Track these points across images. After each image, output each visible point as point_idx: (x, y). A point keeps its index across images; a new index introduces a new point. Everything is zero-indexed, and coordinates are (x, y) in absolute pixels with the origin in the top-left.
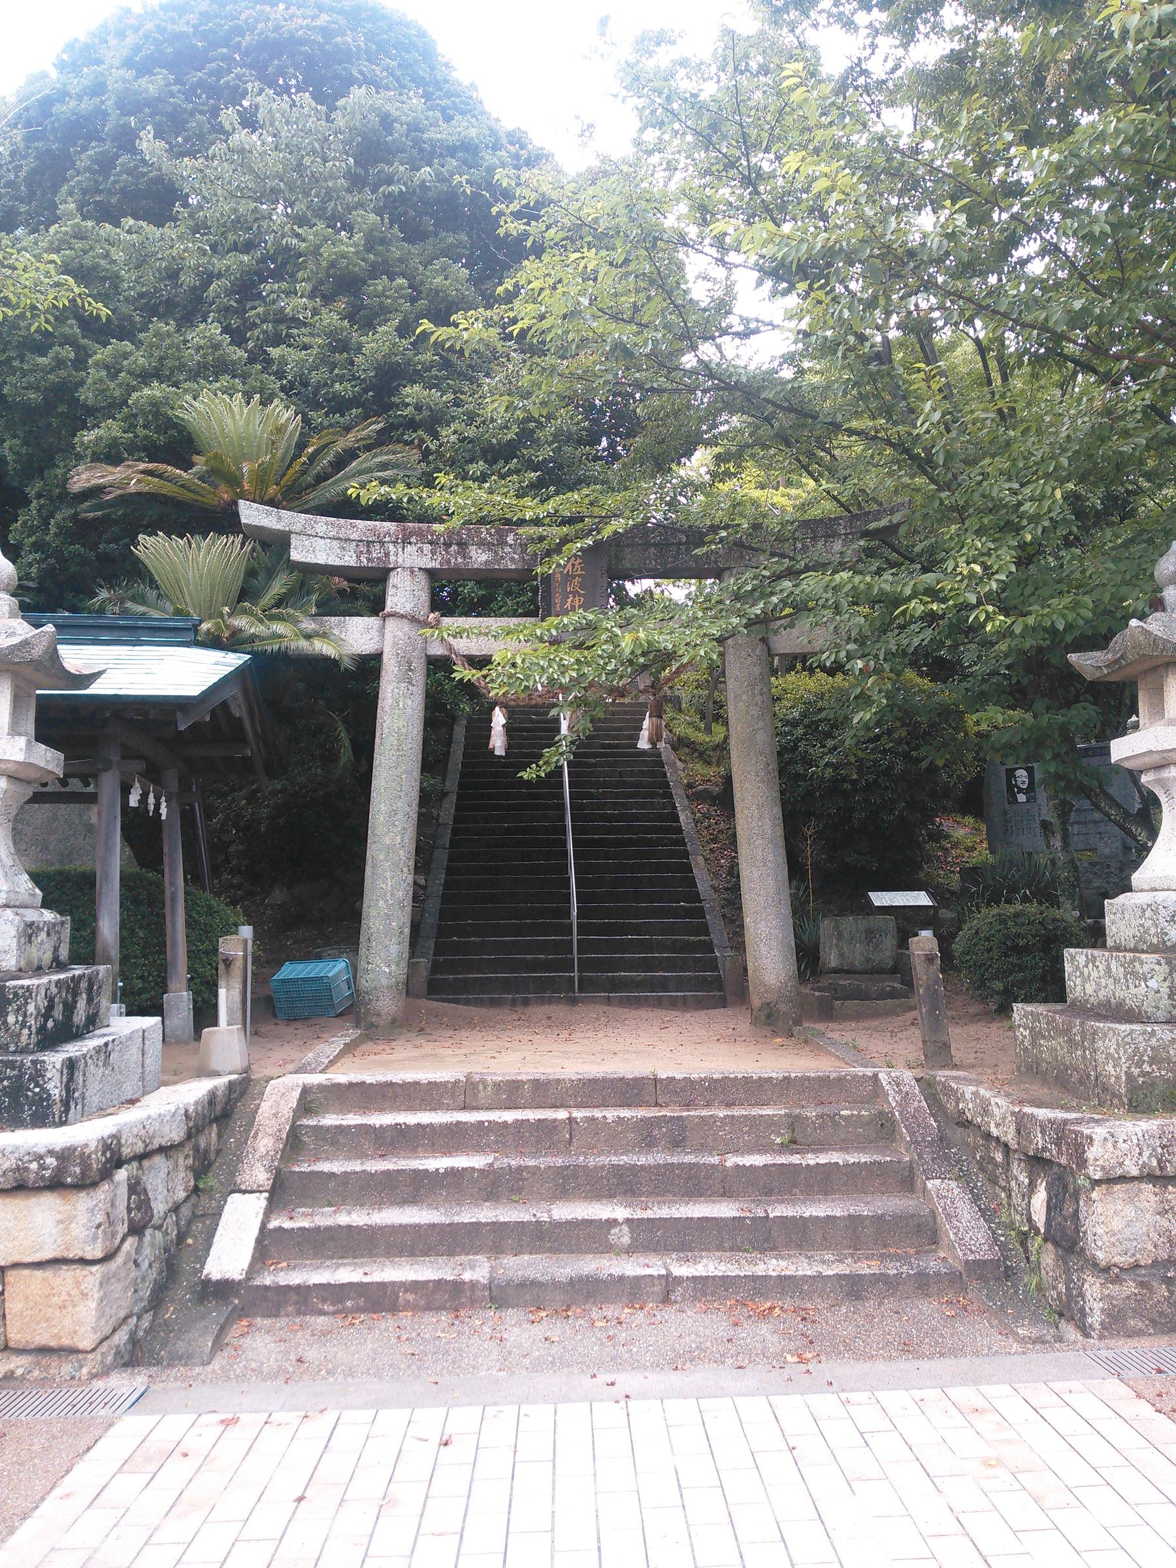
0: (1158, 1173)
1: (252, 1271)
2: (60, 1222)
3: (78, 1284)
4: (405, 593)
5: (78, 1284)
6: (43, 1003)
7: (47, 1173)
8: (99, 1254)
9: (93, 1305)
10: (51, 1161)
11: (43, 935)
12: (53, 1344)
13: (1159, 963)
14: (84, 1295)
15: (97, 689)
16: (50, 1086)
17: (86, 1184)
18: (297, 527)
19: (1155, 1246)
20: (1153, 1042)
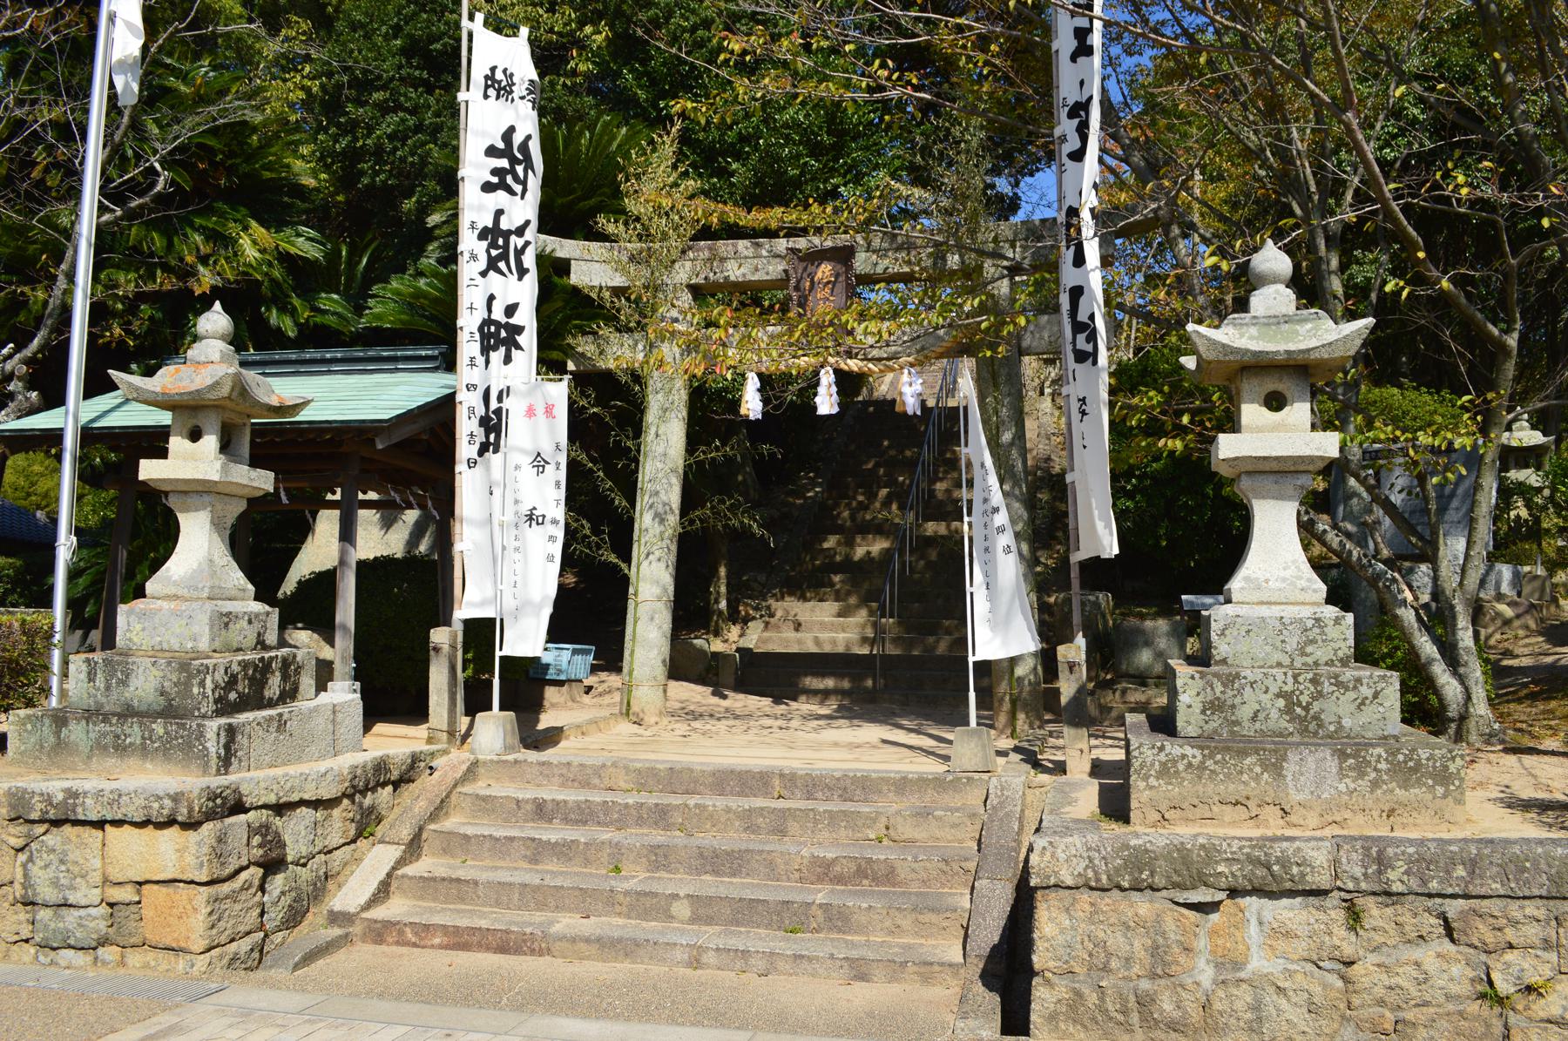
0: (1093, 884)
1: (368, 906)
2: (178, 851)
3: (190, 900)
4: (678, 311)
5: (190, 900)
6: (220, 677)
7: (165, 812)
8: (204, 879)
9: (201, 918)
10: (168, 803)
11: (244, 623)
12: (174, 945)
13: (1193, 677)
14: (195, 910)
15: (305, 415)
16: (208, 745)
17: (191, 825)
18: (577, 254)
19: (1091, 955)
20: (1162, 757)
